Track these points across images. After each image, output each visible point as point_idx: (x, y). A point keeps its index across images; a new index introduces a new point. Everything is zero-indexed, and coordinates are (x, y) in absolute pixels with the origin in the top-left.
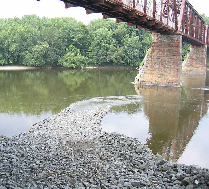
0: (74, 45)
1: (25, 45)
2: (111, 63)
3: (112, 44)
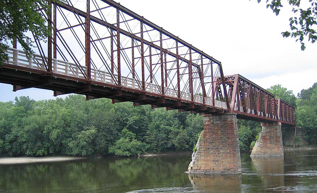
0: (127, 128)
1: (68, 130)
2: (173, 148)
3: (173, 126)
